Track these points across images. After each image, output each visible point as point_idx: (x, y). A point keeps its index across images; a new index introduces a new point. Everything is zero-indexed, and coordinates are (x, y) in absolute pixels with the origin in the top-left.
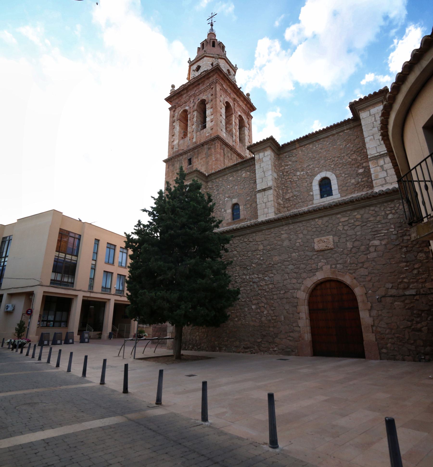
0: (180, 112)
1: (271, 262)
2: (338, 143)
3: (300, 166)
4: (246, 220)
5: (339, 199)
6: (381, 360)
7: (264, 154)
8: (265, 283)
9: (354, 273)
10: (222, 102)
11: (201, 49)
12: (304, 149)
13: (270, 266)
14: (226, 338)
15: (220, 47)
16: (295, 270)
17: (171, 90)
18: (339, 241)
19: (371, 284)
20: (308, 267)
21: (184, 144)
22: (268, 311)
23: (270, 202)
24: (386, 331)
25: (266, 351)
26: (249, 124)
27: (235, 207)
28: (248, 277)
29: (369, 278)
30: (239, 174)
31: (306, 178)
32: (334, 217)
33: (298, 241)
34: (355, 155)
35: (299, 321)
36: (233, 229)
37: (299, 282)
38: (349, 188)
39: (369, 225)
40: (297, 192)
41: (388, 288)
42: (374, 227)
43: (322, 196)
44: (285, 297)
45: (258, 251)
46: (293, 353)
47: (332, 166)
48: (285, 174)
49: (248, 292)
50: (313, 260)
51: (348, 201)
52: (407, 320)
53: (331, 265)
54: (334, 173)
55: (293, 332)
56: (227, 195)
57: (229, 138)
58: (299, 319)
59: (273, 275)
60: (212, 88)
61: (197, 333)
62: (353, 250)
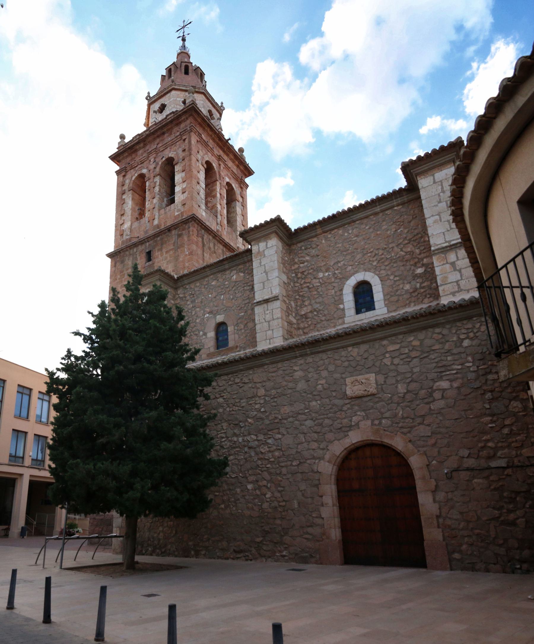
0: (134, 178)
1: (277, 416)
3: (323, 264)
4: (238, 349)
5: (386, 316)
7: (267, 245)
8: (268, 449)
9: (409, 432)
10: (200, 162)
11: (167, 78)
12: (329, 236)
13: (276, 421)
14: (206, 537)
15: (197, 74)
16: (316, 428)
17: (119, 143)
18: (385, 382)
19: (436, 450)
20: (336, 423)
22: (272, 493)
23: (276, 321)
24: (459, 524)
25: (270, 557)
26: (242, 197)
27: (221, 329)
28: (240, 439)
29: (433, 441)
30: (227, 276)
31: (333, 282)
32: (377, 345)
33: (319, 382)
34: (411, 246)
35: (322, 509)
36: (218, 363)
37: (321, 447)
38: (401, 298)
40: (318, 305)
41: (463, 457)
43: (358, 311)
44: (300, 471)
45: (257, 399)
47: (375, 263)
49: (242, 463)
50: (343, 413)
53: (373, 421)
54: (377, 275)
55: (311, 526)
58: (322, 505)
59: (280, 436)
60: (184, 140)
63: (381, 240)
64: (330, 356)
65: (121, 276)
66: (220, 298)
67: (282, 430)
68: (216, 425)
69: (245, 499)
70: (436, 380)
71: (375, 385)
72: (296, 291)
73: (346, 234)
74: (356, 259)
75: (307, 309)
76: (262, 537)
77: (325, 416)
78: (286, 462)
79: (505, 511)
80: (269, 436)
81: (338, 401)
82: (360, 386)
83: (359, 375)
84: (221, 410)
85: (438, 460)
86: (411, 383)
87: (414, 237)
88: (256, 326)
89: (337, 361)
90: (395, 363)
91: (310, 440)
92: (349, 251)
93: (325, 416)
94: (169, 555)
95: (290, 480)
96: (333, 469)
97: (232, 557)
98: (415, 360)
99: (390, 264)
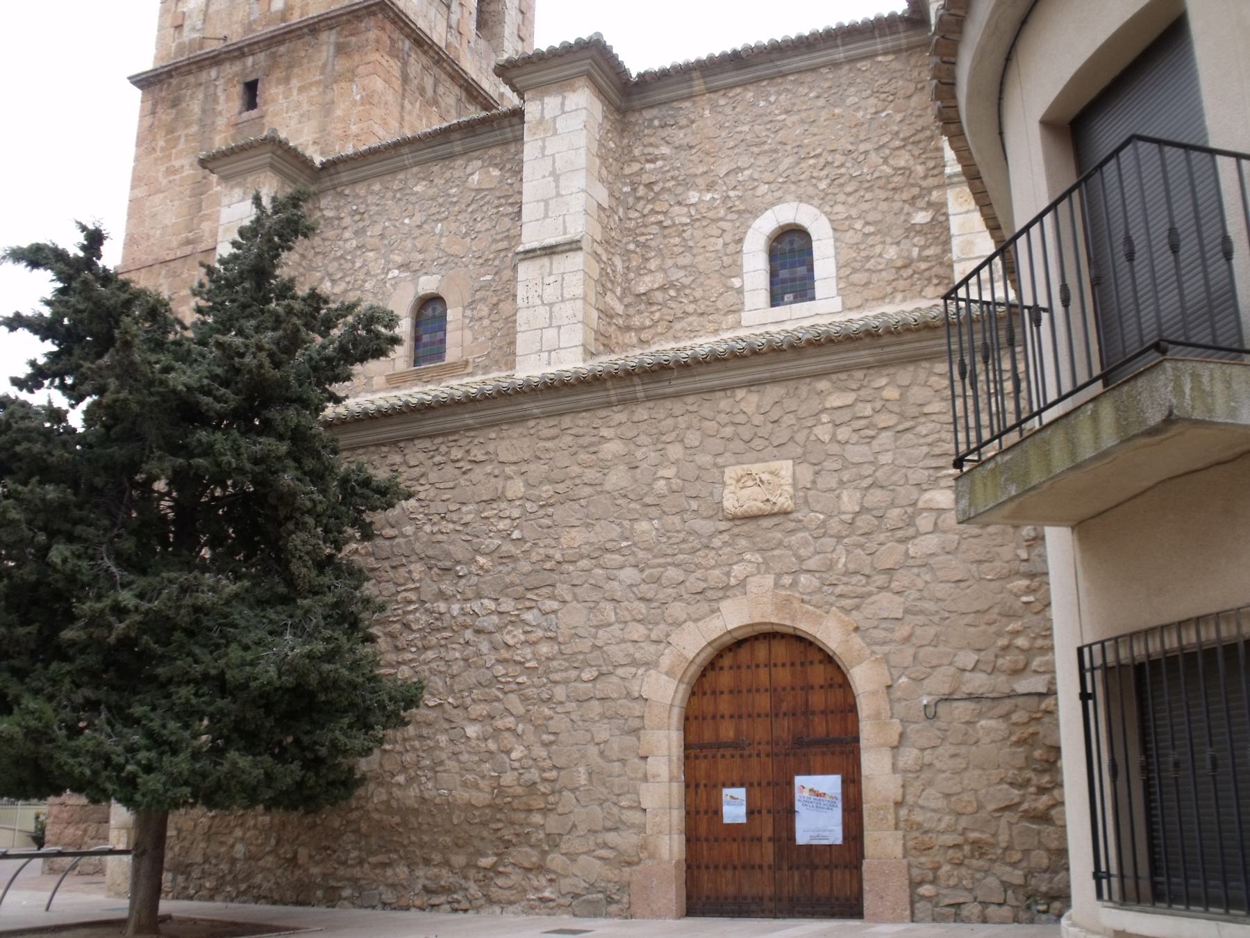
1: (551, 552)
2: (850, 101)
3: (701, 169)
4: (470, 369)
5: (837, 319)
6: (913, 921)
7: (563, 104)
8: (522, 638)
9: (857, 607)
12: (722, 102)
13: (548, 565)
14: (354, 854)
16: (644, 587)
18: (814, 482)
19: (911, 651)
20: (692, 578)
21: (230, 14)
22: (527, 747)
23: (568, 305)
24: (940, 820)
25: (511, 903)
27: (429, 312)
28: (455, 609)
29: (904, 630)
30: (457, 174)
31: (721, 219)
32: (804, 389)
33: (659, 474)
34: (907, 156)
35: (643, 787)
36: (407, 404)
37: (654, 636)
38: (875, 278)
39: (923, 430)
40: (682, 273)
41: (964, 670)
42: (940, 440)
43: (775, 300)
45: (504, 505)
46: (614, 908)
47: (823, 185)
48: (641, 191)
49: (455, 669)
51: (857, 332)
52: (1011, 784)
53: (779, 576)
54: (826, 213)
55: (616, 829)
56: (398, 259)
57: (432, 11)
58: (645, 779)
59: (555, 605)
61: (238, 833)
62: (859, 523)
63: (841, 130)
64: (691, 408)
65: (167, 141)
66: (433, 229)
67: (563, 590)
68: (393, 568)
69: (459, 761)
70: (925, 487)
71: (791, 490)
72: (630, 230)
73: (762, 104)
74: (782, 168)
75: (653, 282)
76: (496, 855)
77: (669, 560)
78: (566, 670)
79: (1032, 789)
80: (528, 604)
81: (703, 522)
82: (757, 488)
83: (756, 462)
84: (409, 529)
85: (913, 676)
86: (871, 491)
87: (914, 135)
88: (518, 315)
89: (707, 423)
90: (839, 438)
91: (628, 618)
92: (766, 147)
93: (669, 560)
94: (257, 899)
95: (573, 717)
96: (676, 692)
97: (418, 903)
98: (884, 434)
99: (856, 191)
